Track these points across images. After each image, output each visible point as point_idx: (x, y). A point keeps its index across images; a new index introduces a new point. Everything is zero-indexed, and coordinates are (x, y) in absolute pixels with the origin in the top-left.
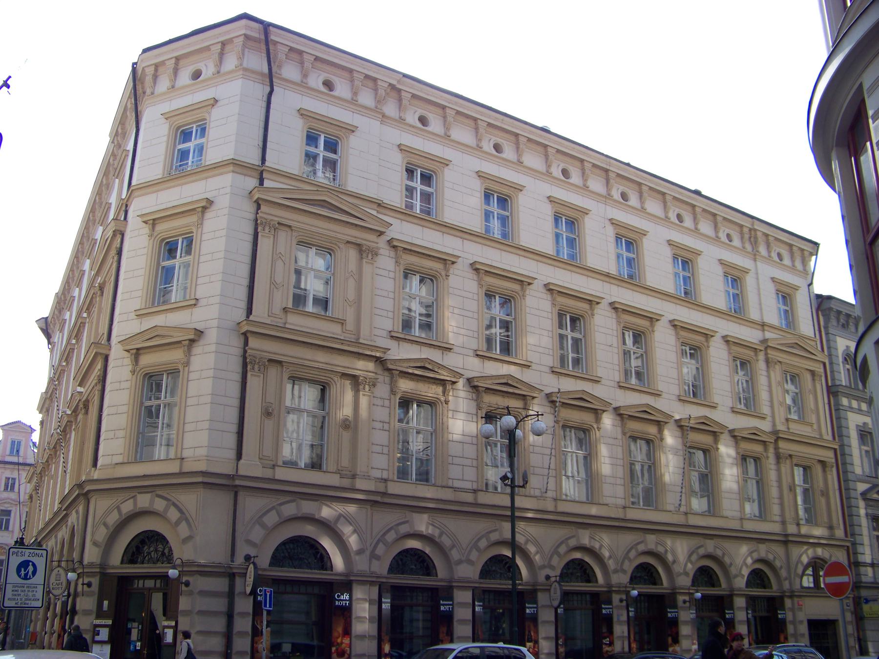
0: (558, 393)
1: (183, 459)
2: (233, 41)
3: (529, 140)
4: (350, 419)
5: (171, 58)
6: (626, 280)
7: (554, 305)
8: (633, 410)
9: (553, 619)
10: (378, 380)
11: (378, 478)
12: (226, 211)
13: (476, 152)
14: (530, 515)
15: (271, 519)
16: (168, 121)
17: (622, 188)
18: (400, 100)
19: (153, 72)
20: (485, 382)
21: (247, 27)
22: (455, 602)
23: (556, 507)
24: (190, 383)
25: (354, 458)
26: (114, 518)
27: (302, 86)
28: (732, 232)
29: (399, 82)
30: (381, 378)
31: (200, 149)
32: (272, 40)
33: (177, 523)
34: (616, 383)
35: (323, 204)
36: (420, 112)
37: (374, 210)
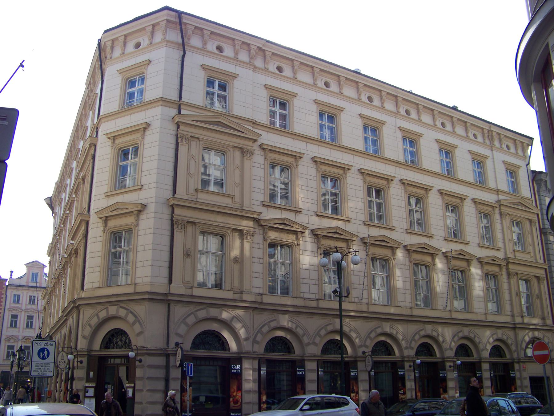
1: (136, 284)
3: (347, 79)
4: (239, 257)
7: (364, 182)
11: (257, 293)
12: (158, 130)
14: (352, 314)
15: (191, 320)
16: (121, 75)
17: (406, 107)
18: (265, 57)
21: (168, 15)
23: (368, 308)
25: (241, 281)
27: (203, 50)
28: (283, 65)
29: (263, 45)
30: (257, 231)
31: (141, 92)
32: (184, 22)
33: (134, 323)
36: (278, 64)
37: (251, 126)
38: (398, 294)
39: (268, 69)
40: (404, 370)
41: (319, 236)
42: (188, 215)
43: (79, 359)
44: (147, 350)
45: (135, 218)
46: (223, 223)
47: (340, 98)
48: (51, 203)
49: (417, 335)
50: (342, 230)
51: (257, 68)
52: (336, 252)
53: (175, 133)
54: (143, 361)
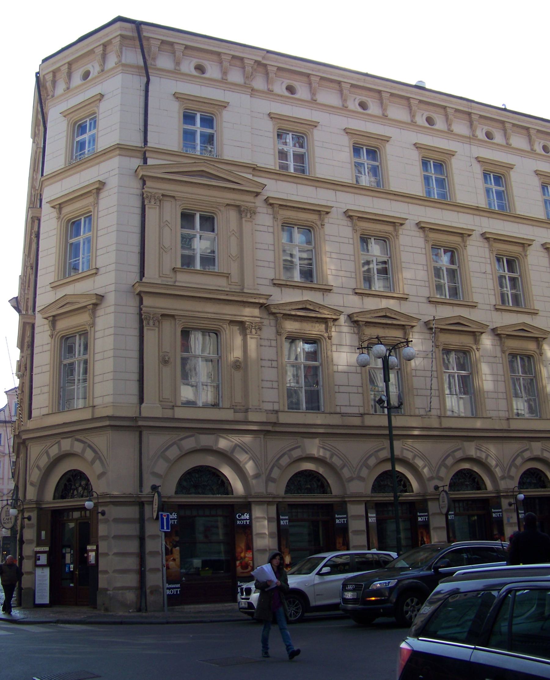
0: (434, 320)
1: (95, 406)
2: (112, 42)
3: (392, 95)
4: (240, 360)
5: (65, 64)
7: (426, 241)
8: (510, 330)
9: (444, 525)
10: (264, 324)
11: (270, 410)
12: (116, 190)
13: (411, 127)
14: (416, 433)
15: (174, 453)
16: (66, 118)
17: (486, 128)
18: (267, 74)
19: (51, 78)
20: (364, 316)
21: (121, 28)
22: (349, 515)
23: (440, 423)
24: (96, 341)
25: (246, 395)
26: (44, 462)
28: (369, 99)
29: (264, 58)
30: (266, 322)
31: (93, 139)
32: (145, 36)
33: (93, 462)
34: (492, 307)
35: (202, 174)
36: (287, 82)
37: (250, 174)
38: (487, 400)
39: (416, 123)
40: (500, 510)
41: (360, 323)
42: (189, 308)
43: (26, 515)
44: (110, 497)
45: (89, 314)
46: (215, 313)
47: (347, 116)
48: (16, 304)
49: (450, 458)
50: (394, 312)
51: (257, 91)
52: (378, 344)
53: (139, 192)
54: (106, 512)
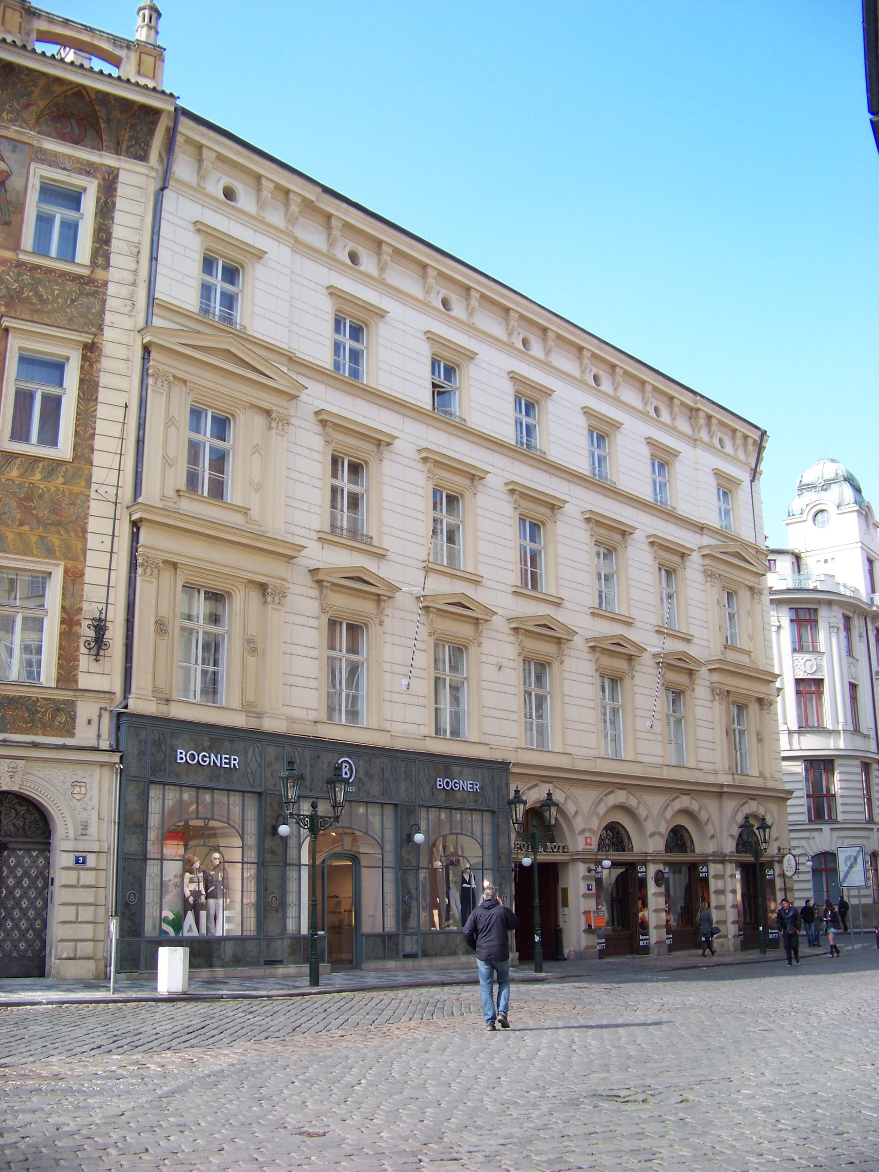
6: (346, 380)
8: (529, 623)
17: (351, 246)
27: (198, 192)
28: (531, 335)
